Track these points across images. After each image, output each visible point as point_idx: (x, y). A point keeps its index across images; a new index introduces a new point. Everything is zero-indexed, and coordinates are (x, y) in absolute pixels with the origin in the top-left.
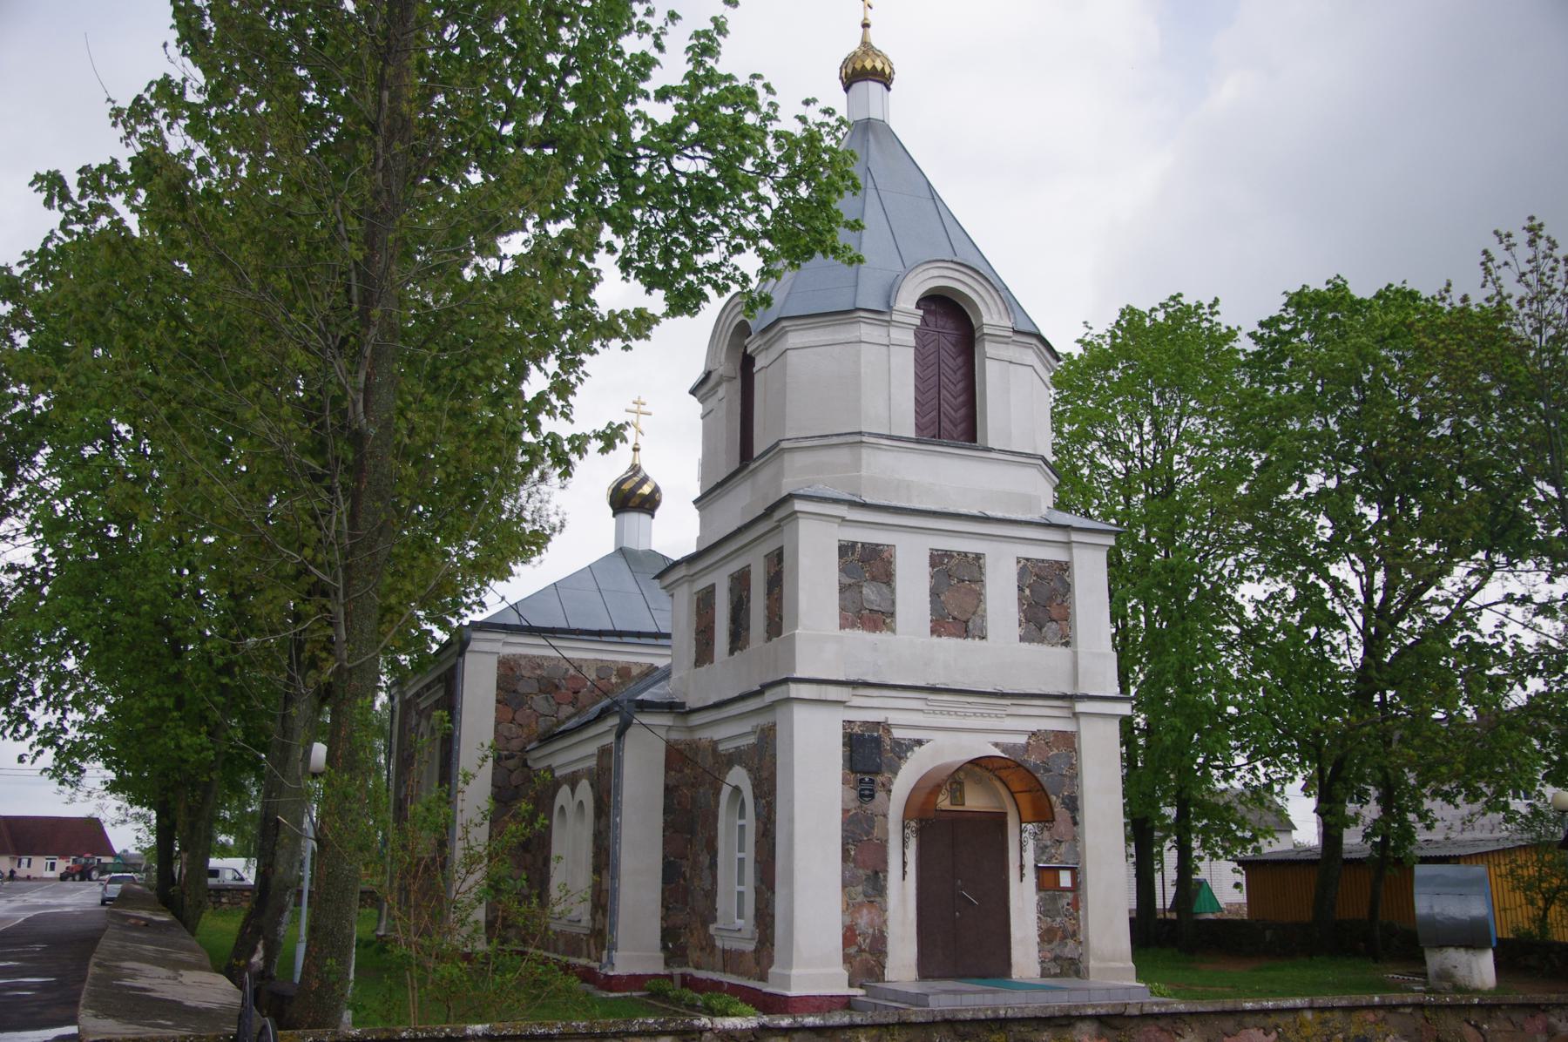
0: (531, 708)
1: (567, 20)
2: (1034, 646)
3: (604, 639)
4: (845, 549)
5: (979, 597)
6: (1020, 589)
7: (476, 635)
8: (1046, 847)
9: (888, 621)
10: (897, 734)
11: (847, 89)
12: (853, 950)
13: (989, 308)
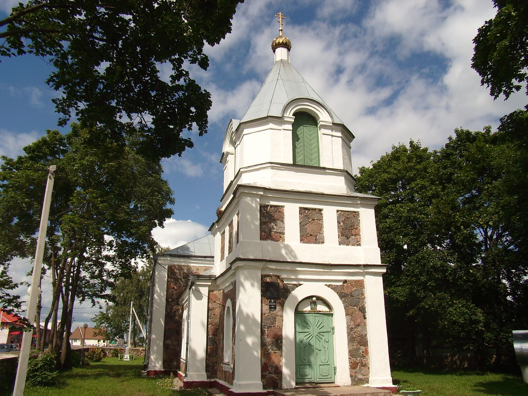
1: (477, 329)
2: (345, 247)
3: (206, 259)
5: (321, 227)
6: (339, 222)
8: (352, 328)
12: (266, 373)
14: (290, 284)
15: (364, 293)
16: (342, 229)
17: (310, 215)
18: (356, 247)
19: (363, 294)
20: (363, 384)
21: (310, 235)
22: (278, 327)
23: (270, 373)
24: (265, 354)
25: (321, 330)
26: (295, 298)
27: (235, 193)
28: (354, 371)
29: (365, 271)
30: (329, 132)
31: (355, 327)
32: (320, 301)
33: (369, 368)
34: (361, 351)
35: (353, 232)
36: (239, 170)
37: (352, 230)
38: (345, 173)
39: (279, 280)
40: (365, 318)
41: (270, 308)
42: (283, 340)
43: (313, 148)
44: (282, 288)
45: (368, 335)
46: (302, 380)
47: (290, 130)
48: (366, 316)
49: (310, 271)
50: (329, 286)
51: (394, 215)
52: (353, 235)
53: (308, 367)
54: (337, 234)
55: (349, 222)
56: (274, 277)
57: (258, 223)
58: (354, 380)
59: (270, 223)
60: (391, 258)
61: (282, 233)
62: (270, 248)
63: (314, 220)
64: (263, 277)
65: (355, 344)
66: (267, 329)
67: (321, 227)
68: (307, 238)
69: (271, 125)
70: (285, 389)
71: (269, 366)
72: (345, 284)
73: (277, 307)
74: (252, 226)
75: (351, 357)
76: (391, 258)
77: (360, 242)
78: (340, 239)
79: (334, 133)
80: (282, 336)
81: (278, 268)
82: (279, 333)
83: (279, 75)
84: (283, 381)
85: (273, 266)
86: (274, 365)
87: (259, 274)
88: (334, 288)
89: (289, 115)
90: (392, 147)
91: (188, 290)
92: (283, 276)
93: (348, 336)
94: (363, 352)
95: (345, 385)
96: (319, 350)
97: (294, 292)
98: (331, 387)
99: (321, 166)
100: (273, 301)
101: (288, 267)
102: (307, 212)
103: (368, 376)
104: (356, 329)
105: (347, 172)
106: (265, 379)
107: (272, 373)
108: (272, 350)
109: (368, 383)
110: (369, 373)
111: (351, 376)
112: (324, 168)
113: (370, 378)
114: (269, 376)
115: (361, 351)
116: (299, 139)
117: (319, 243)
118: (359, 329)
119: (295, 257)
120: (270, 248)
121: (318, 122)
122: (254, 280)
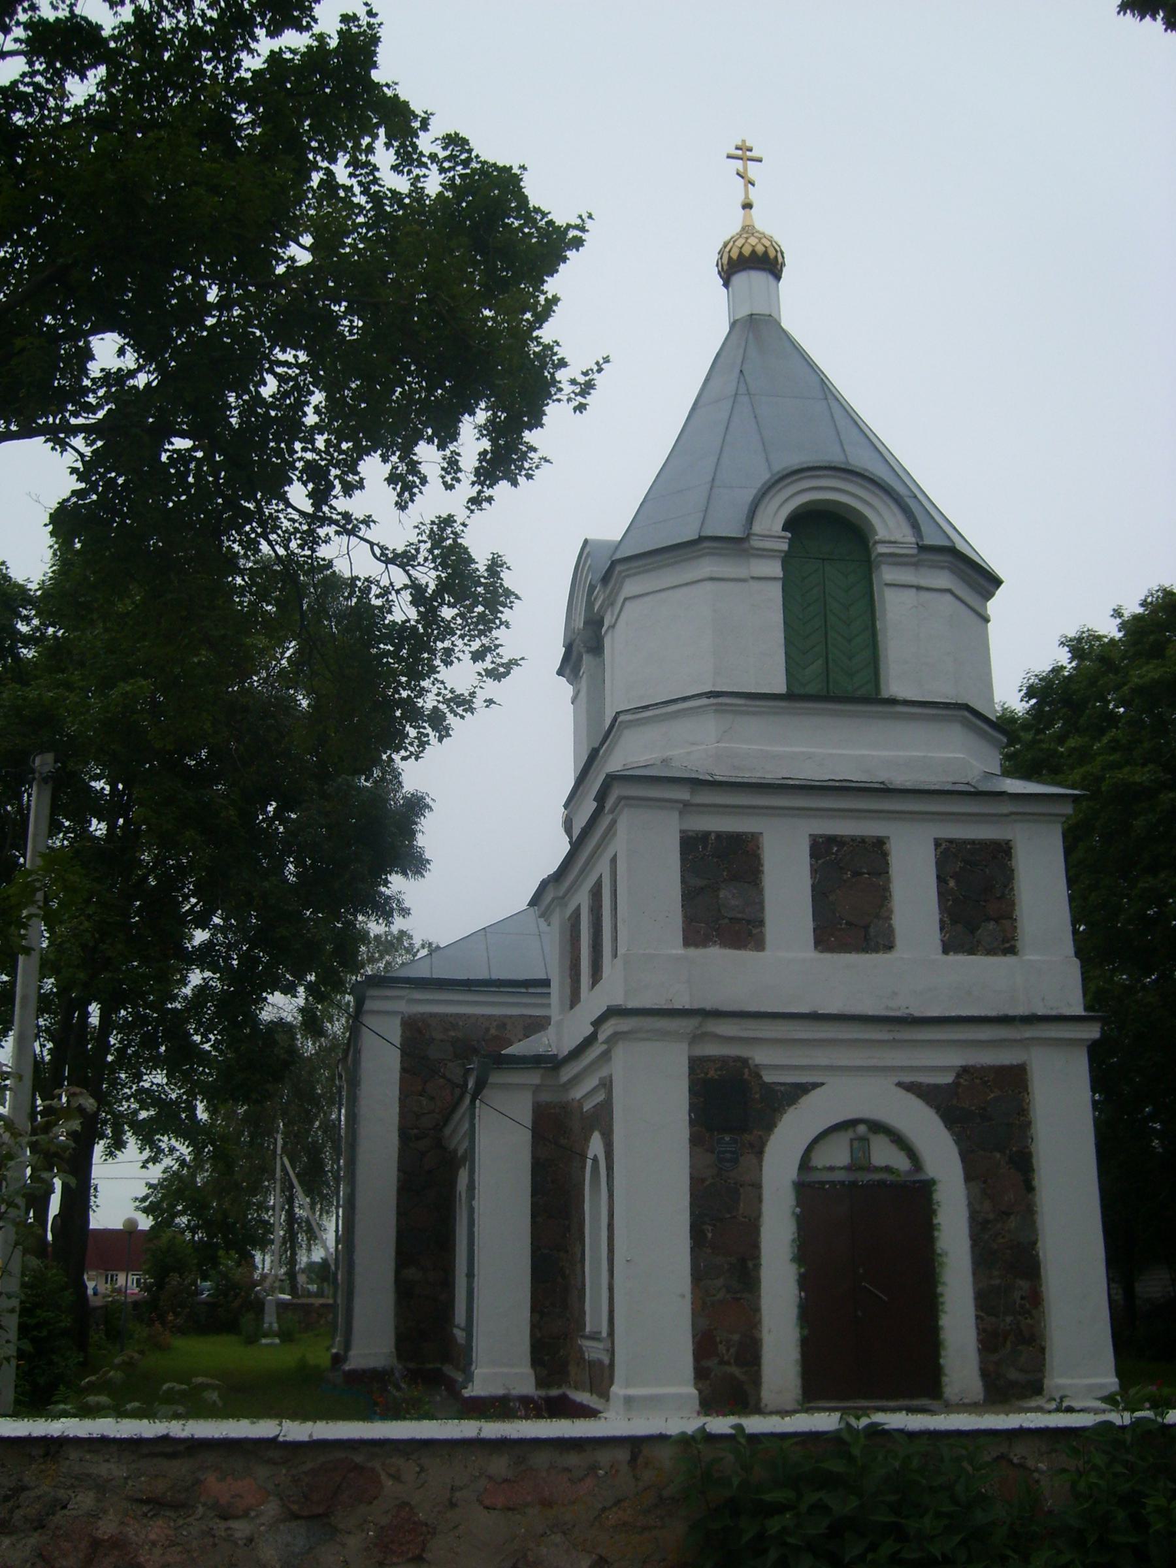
0: (444, 1077)
3: (531, 990)
4: (691, 845)
6: (941, 879)
7: (372, 992)
9: (755, 931)
10: (768, 1078)
11: (726, 284)
12: (712, 1363)
13: (879, 515)
15: (1026, 1107)
21: (846, 924)
23: (722, 1362)
27: (601, 798)
36: (615, 719)
37: (985, 901)
47: (775, 579)
50: (910, 1088)
54: (937, 917)
65: (996, 1273)
67: (883, 895)
71: (718, 1339)
75: (982, 1314)
78: (947, 933)
83: (742, 379)
91: (467, 1101)
95: (966, 1401)
99: (885, 694)
100: (727, 1139)
102: (835, 849)
107: (728, 1363)
112: (893, 702)
118: (1012, 1223)
121: (871, 544)
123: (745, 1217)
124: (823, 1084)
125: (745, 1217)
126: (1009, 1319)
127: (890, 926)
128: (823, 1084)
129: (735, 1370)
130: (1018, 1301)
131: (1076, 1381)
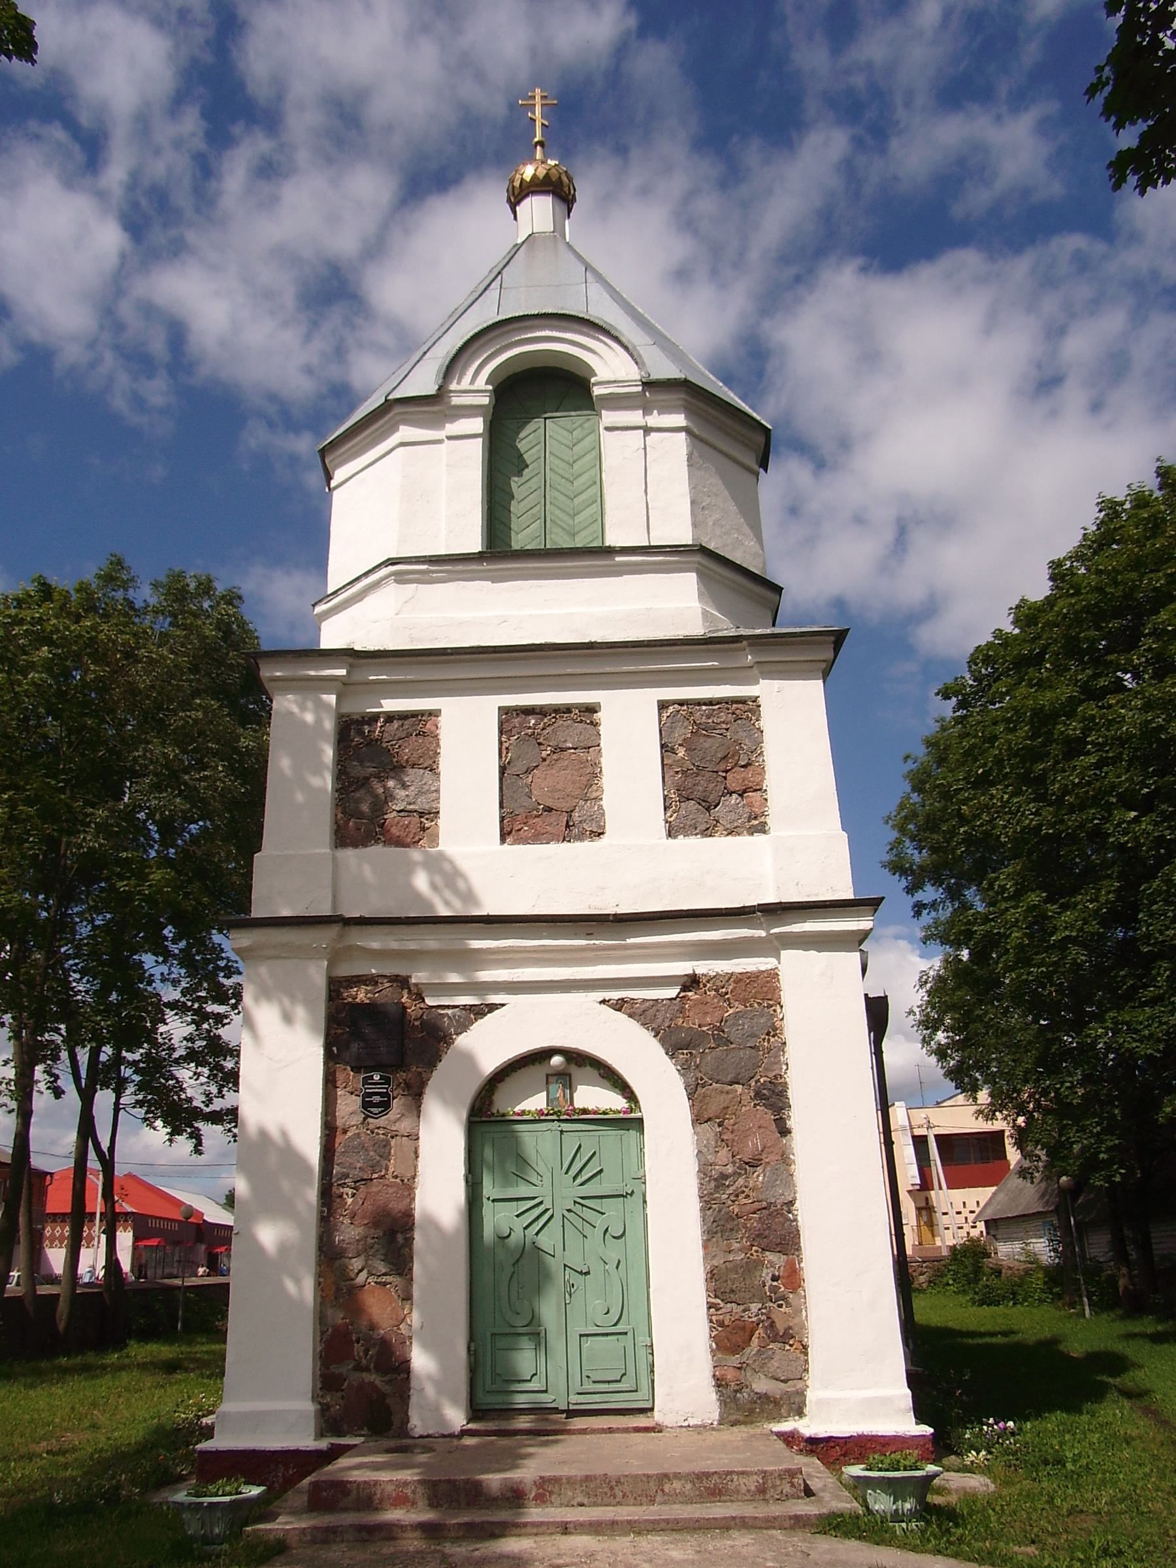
5: (593, 774)
8: (724, 1176)
12: (345, 1369)
14: (448, 1007)
15: (778, 1024)
16: (683, 772)
17: (545, 732)
18: (745, 839)
19: (773, 1031)
20: (779, 1418)
22: (398, 1180)
23: (359, 1368)
24: (338, 1289)
25: (591, 1189)
26: (468, 1060)
28: (735, 1360)
29: (772, 931)
30: (635, 417)
31: (735, 1173)
32: (588, 1068)
33: (805, 1347)
34: (766, 1274)
35: (735, 780)
38: (698, 558)
39: (405, 992)
40: (785, 1132)
41: (366, 1105)
42: (417, 1235)
43: (581, 489)
44: (417, 1023)
45: (797, 1205)
46: (499, 1398)
48: (791, 1123)
49: (535, 950)
50: (618, 1005)
51: (1100, 740)
52: (731, 793)
53: (526, 1343)
55: (711, 745)
56: (389, 984)
57: (326, 782)
58: (735, 1399)
59: (382, 780)
60: (1103, 899)
61: (430, 813)
62: (367, 871)
63: (563, 750)
64: (336, 987)
65: (736, 1246)
66: (350, 1191)
68: (531, 822)
69: (406, 432)
70: (421, 1437)
72: (690, 994)
73: (395, 1103)
74: (300, 797)
76: (1103, 899)
77: (762, 819)
79: (655, 420)
80: (412, 1216)
81: (394, 945)
82: (397, 1206)
83: (499, 277)
84: (414, 1400)
85: (375, 941)
86: (375, 1336)
87: (317, 974)
88: (642, 1013)
89: (607, 429)
90: (1098, 504)
92: (416, 977)
93: (702, 1209)
94: (774, 1279)
95: (692, 1422)
96: (581, 1273)
97: (463, 1041)
98: (594, 1431)
100: (377, 1078)
101: (431, 940)
102: (533, 722)
103: (800, 1384)
104: (741, 1181)
105: (703, 551)
106: (339, 1394)
107: (367, 1369)
108: (370, 1274)
109: (800, 1413)
110: (806, 1370)
111: (720, 1383)
113: (809, 1394)
114: (355, 1378)
115: (766, 1274)
116: (527, 466)
117: (580, 837)
118: (759, 1177)
119: (469, 896)
120: (367, 871)
122: (293, 998)
123: (396, 1177)
124: (503, 1005)
125: (396, 1177)
126: (755, 1307)
127: (601, 807)
128: (503, 1005)
129: (374, 1378)
130: (769, 1283)
131: (846, 1394)
